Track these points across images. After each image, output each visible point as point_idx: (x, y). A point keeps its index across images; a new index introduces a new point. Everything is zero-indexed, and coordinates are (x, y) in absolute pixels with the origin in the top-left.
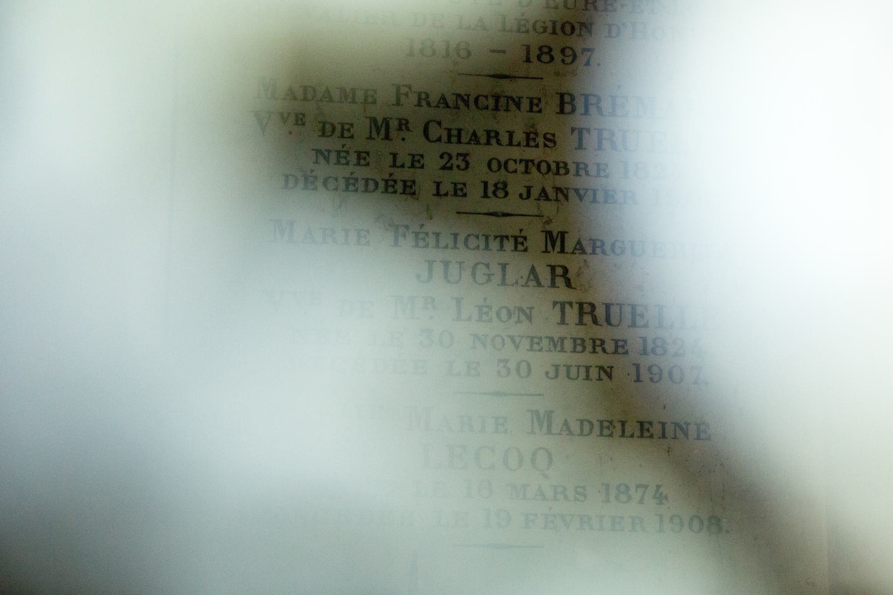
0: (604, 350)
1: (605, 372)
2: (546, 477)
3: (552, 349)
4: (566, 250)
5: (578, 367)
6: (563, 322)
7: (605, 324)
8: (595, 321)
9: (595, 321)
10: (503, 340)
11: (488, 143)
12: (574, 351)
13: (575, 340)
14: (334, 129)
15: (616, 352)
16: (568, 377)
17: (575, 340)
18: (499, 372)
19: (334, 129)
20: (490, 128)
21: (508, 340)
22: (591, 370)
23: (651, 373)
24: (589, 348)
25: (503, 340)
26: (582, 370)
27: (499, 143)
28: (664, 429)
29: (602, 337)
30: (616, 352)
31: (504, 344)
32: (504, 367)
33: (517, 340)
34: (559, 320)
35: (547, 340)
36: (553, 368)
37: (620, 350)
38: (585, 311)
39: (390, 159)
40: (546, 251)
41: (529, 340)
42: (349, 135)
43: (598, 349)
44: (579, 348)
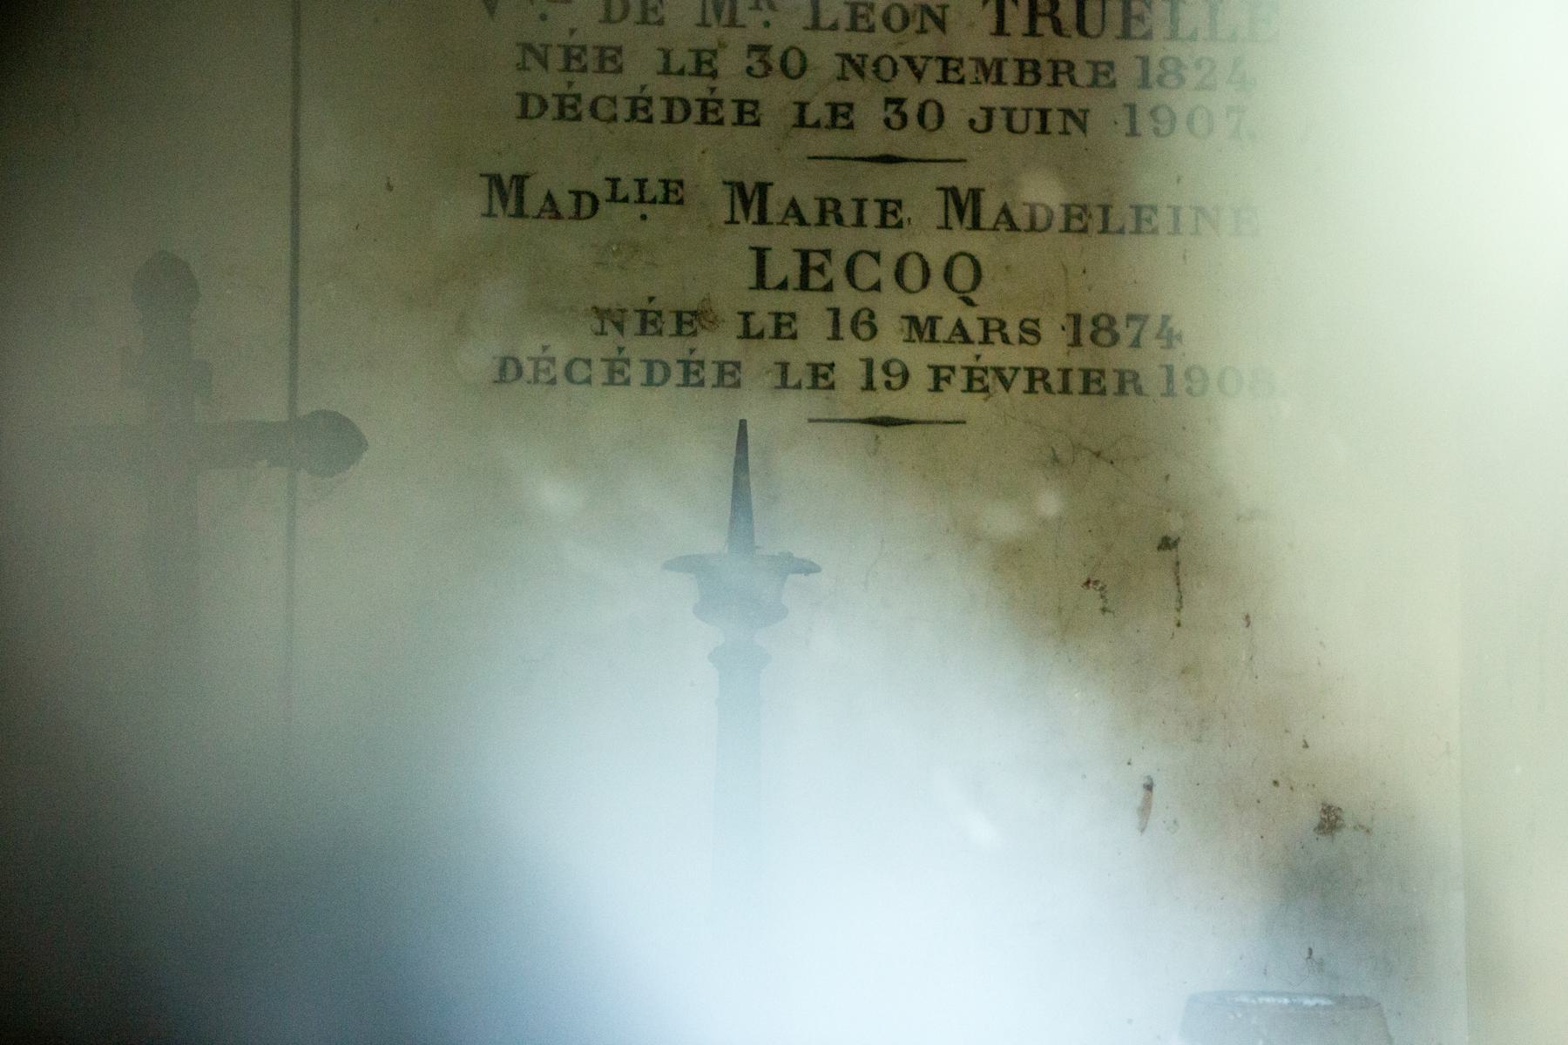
0: (1073, 81)
1: (1075, 119)
2: (970, 303)
3: (982, 78)
4: (983, 224)
5: (1028, 110)
6: (1000, 30)
7: (1075, 34)
8: (1058, 29)
9: (1058, 29)
10: (895, 65)
11: (822, 222)
12: (1021, 82)
13: (1021, 62)
14: (544, 105)
15: (1095, 83)
16: (1010, 128)
17: (1021, 62)
18: (887, 122)
19: (544, 105)
20: (824, 195)
21: (903, 65)
22: (1050, 116)
23: (1156, 120)
24: (1047, 77)
25: (895, 65)
26: (1035, 117)
27: (839, 220)
28: (1170, 379)
29: (1069, 58)
30: (1095, 83)
31: (895, 72)
32: (897, 111)
33: (919, 63)
34: (993, 27)
35: (973, 63)
36: (984, 113)
37: (1103, 80)
38: (1040, 10)
39: (658, 58)
40: (947, 226)
41: (940, 63)
42: (548, 379)
43: (1063, 79)
44: (1029, 78)
